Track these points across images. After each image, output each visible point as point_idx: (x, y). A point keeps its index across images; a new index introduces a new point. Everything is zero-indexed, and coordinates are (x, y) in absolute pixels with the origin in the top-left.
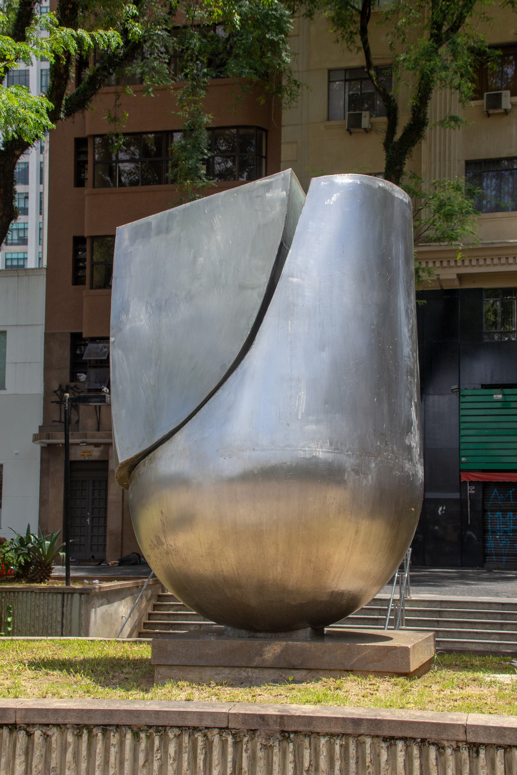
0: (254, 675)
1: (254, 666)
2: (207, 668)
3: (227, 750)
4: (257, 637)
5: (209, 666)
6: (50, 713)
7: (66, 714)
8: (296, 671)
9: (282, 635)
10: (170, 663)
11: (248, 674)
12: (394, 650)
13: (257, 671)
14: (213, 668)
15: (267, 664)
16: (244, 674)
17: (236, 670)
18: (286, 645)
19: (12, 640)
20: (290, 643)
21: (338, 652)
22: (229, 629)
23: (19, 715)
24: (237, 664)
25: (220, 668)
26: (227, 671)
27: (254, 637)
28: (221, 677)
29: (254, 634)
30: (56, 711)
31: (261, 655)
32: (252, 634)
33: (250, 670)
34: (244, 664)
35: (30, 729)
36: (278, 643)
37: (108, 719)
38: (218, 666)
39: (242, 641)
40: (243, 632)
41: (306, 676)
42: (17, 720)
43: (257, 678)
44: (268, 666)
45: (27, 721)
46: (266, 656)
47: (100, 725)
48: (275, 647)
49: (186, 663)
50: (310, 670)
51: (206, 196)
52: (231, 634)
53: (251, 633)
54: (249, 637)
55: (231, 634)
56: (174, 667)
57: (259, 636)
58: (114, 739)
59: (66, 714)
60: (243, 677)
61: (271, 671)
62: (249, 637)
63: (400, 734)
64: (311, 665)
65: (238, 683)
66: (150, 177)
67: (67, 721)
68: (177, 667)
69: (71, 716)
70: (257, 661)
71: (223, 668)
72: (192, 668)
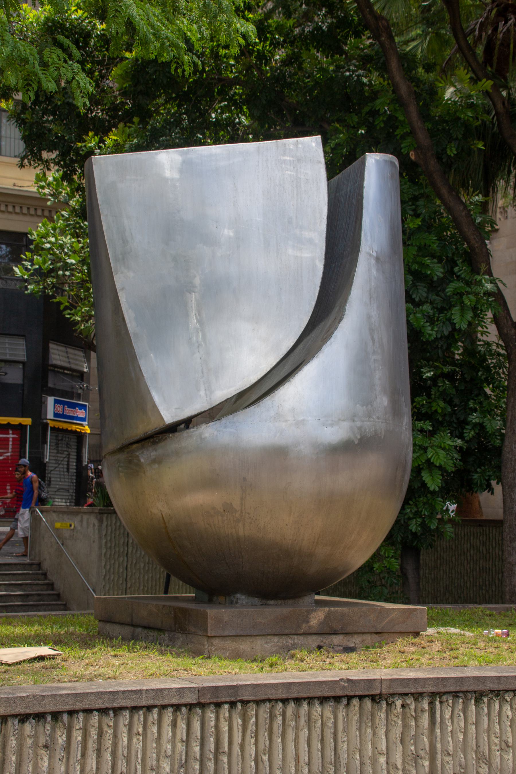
0: (299, 642)
1: (301, 633)
2: (258, 638)
3: (435, 712)
4: (269, 605)
5: (260, 635)
6: (411, 682)
7: (425, 683)
8: (335, 636)
9: (290, 602)
10: (226, 634)
11: (294, 641)
12: (415, 611)
13: (302, 638)
14: (264, 637)
15: (313, 631)
16: (291, 641)
17: (284, 637)
18: (329, 611)
19: (28, 616)
20: (332, 609)
21: (372, 616)
22: (243, 597)
23: (384, 685)
24: (287, 632)
25: (269, 637)
26: (276, 639)
27: (265, 605)
28: (270, 645)
29: (265, 602)
30: (416, 680)
31: (308, 622)
32: (264, 601)
33: (296, 637)
34: (293, 632)
35: (391, 700)
36: (322, 609)
37: (460, 686)
38: (268, 635)
39: (291, 609)
40: (256, 600)
41: (342, 640)
42: (383, 690)
43: (302, 644)
44: (314, 632)
45: (391, 691)
46: (312, 623)
47: (451, 692)
48: (320, 614)
49: (241, 633)
50: (346, 634)
51: (189, 147)
52: (244, 602)
53: (263, 601)
54: (261, 605)
55: (244, 602)
56: (227, 638)
57: (270, 603)
58: (211, 716)
59: (425, 683)
60: (290, 644)
61: (314, 637)
62: (261, 605)
63: (305, 695)
64: (350, 629)
65: (285, 650)
66: (45, 106)
67: (425, 690)
68: (230, 638)
69: (429, 685)
70: (304, 628)
71: (272, 637)
72: (244, 638)
